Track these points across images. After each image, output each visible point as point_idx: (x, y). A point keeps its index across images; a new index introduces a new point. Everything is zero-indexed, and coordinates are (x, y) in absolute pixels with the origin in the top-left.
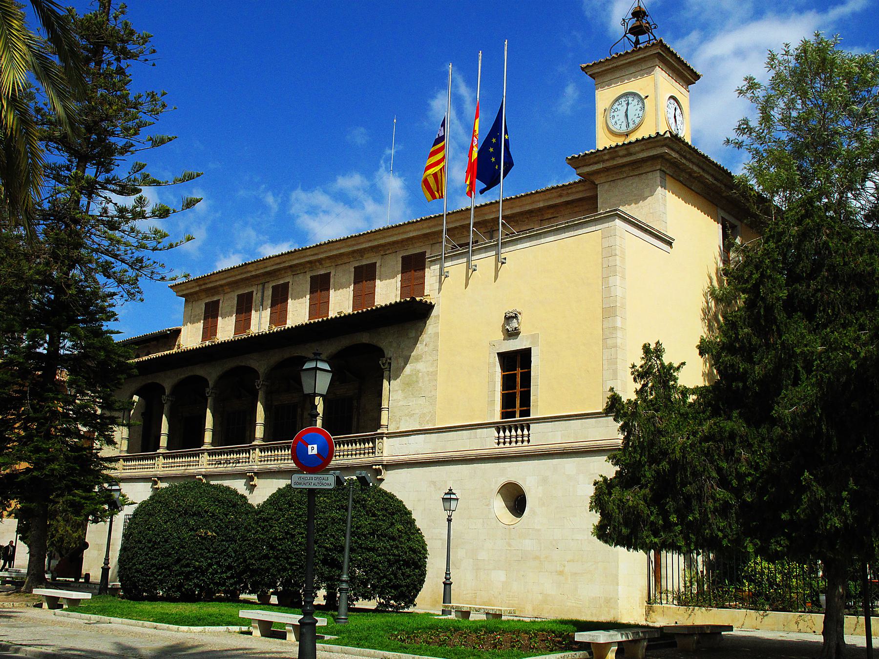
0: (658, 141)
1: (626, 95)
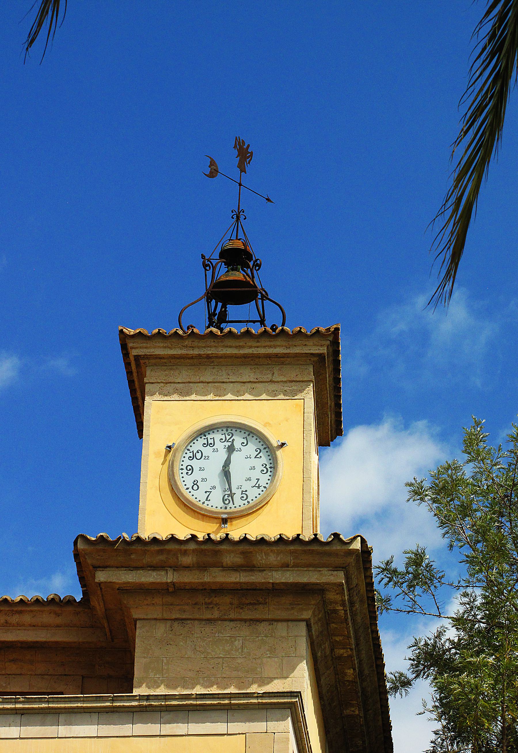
0: (330, 554)
1: (231, 427)
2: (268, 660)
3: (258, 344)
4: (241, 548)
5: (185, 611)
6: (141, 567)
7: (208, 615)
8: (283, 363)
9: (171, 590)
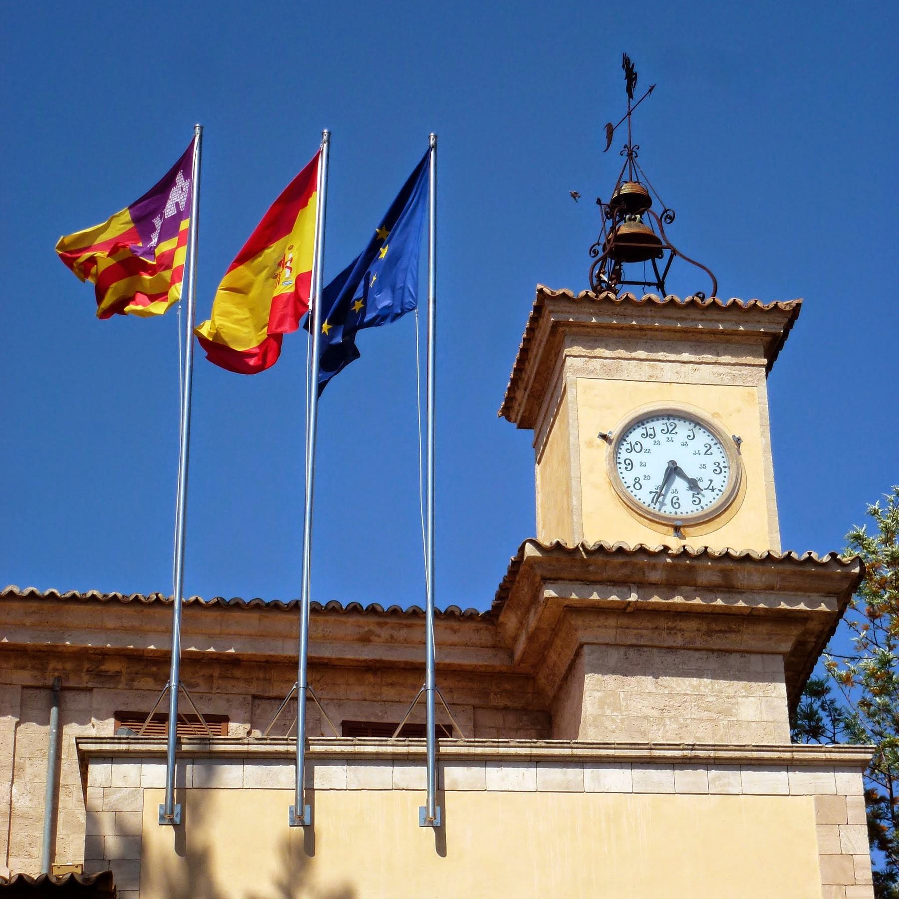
2: (744, 699)
3: (704, 317)
4: (721, 565)
7: (669, 642)
8: (728, 341)
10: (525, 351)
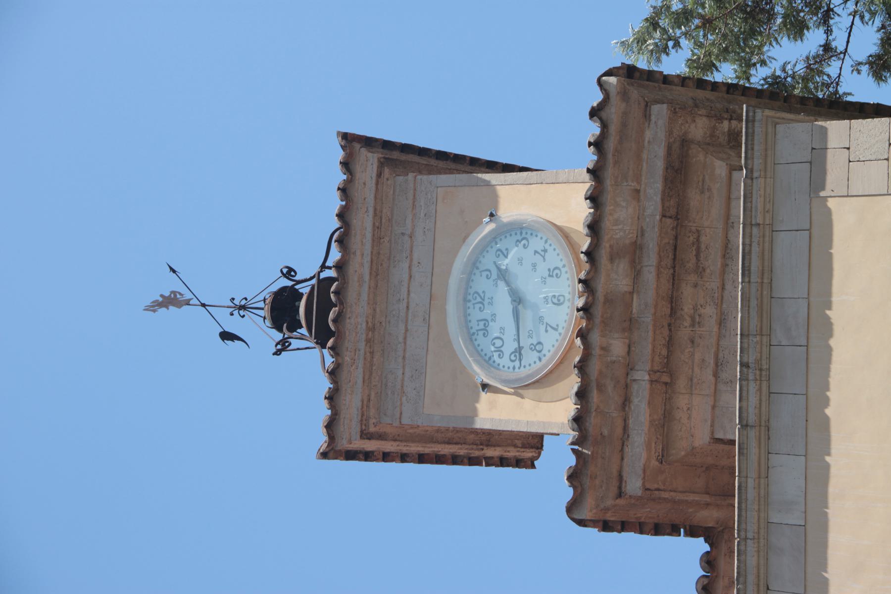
3: (358, 253)
5: (703, 360)
6: (625, 420)
7: (711, 324)
9: (665, 378)
10: (422, 459)
